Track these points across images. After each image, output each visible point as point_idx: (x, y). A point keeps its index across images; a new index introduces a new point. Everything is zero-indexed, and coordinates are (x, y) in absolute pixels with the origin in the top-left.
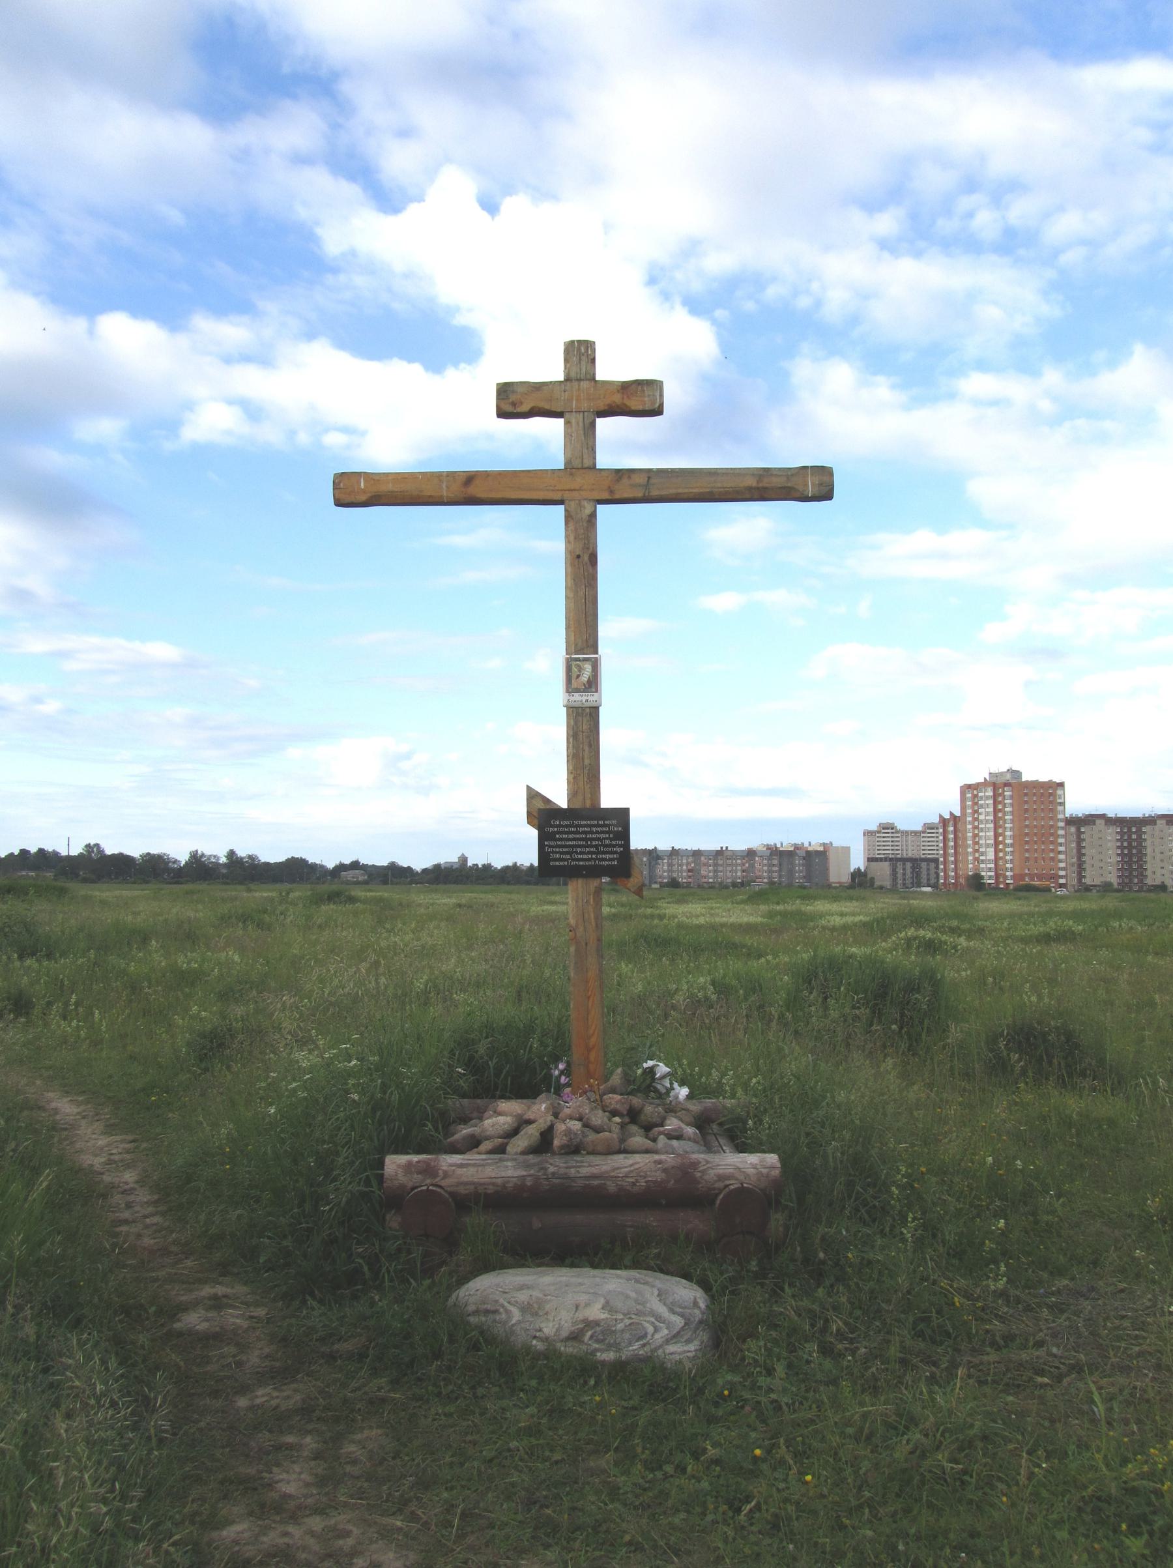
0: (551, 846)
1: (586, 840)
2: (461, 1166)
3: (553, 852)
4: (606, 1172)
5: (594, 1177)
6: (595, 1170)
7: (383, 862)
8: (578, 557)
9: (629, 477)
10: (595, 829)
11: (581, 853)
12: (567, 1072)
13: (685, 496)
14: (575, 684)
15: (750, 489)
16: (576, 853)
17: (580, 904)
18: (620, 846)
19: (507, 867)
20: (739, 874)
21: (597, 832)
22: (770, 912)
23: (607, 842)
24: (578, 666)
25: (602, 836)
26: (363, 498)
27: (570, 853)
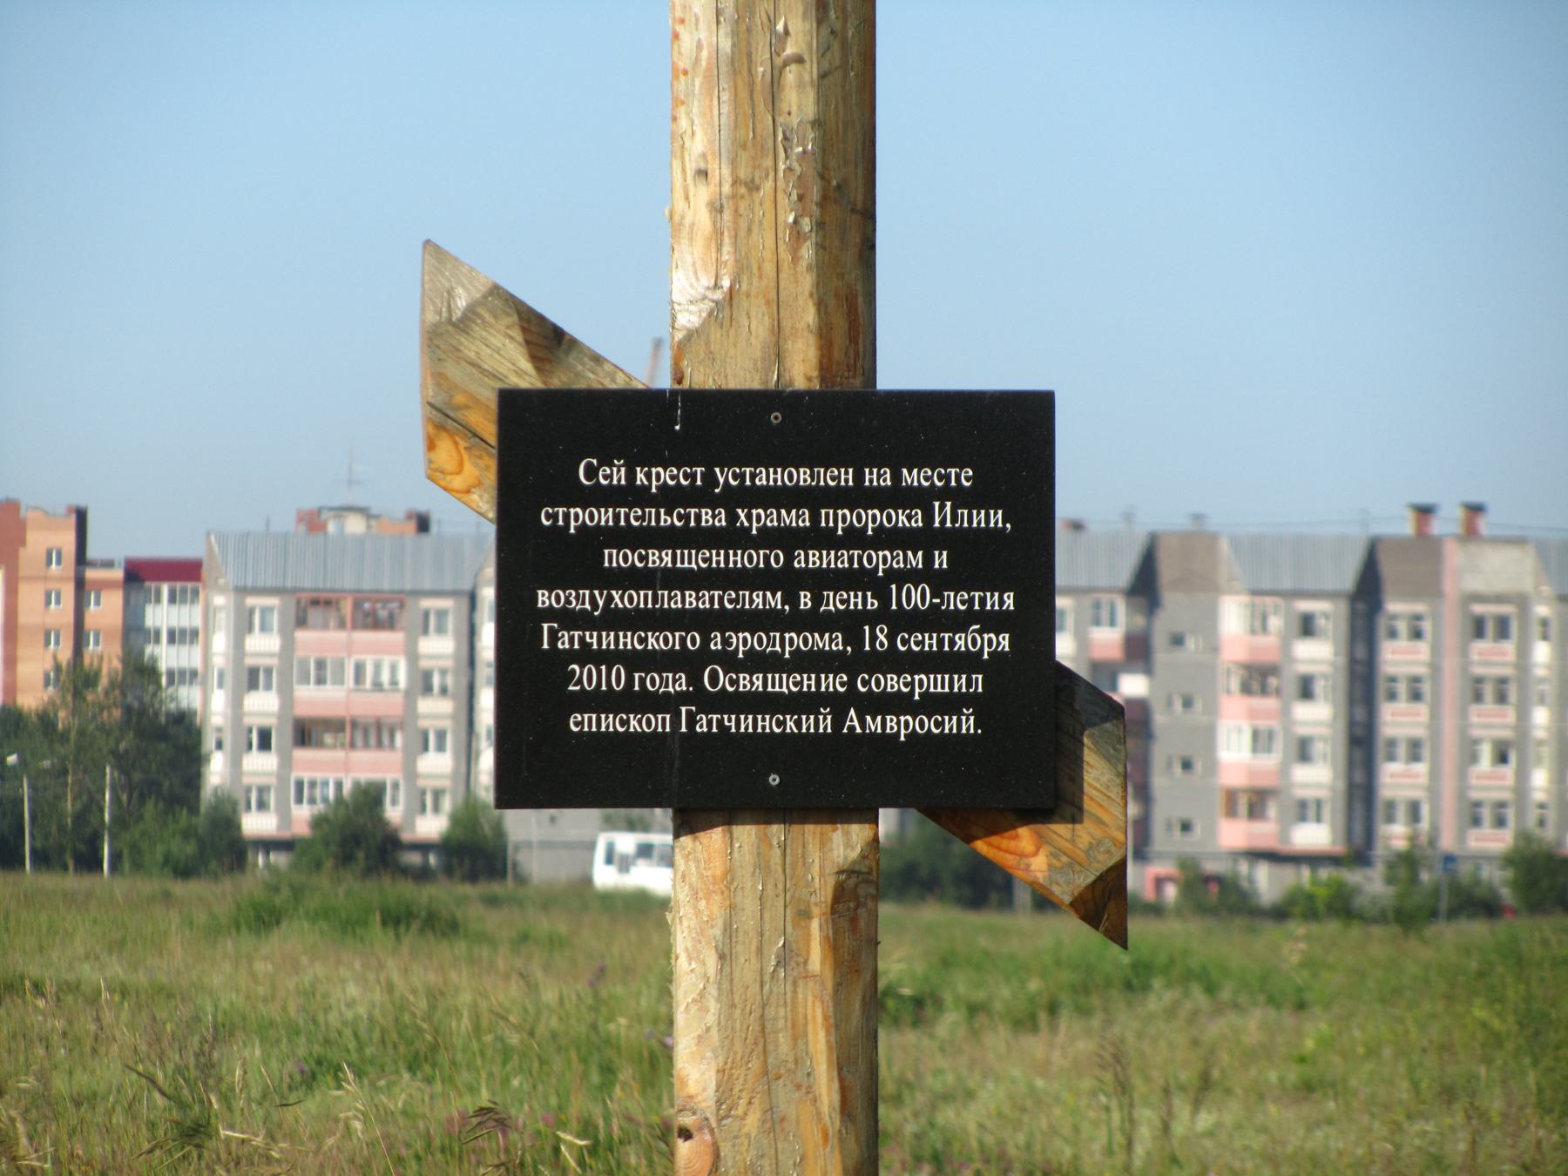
0: (569, 619)
1: (788, 581)
3: (586, 655)
10: (840, 519)
16: (729, 661)
17: (746, 970)
18: (993, 622)
21: (855, 538)
23: (917, 597)
25: (881, 560)
27: (689, 663)
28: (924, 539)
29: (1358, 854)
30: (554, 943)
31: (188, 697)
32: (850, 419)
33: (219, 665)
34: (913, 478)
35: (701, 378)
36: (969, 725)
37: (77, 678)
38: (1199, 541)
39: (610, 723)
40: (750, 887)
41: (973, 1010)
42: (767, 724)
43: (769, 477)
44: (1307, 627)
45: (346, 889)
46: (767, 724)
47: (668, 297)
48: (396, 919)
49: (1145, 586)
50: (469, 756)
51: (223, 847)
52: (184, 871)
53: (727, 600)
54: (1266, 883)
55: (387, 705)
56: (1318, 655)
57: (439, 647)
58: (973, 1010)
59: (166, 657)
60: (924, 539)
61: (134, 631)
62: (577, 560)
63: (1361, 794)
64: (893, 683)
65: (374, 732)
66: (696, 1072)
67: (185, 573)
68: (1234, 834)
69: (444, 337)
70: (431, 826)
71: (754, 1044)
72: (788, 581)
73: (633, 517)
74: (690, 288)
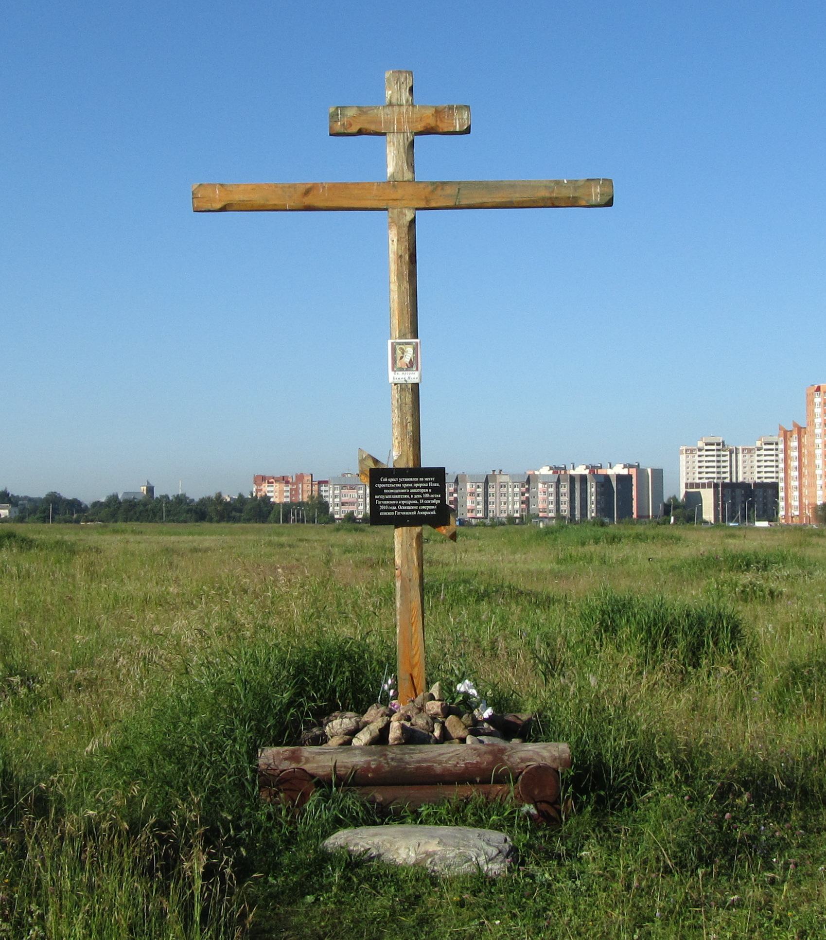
0: (380, 500)
1: (409, 494)
2: (319, 754)
3: (382, 504)
4: (434, 757)
5: (425, 761)
6: (423, 756)
7: (39, 492)
8: (401, 256)
9: (442, 189)
10: (416, 485)
11: (406, 505)
12: (394, 686)
13: (489, 205)
14: (399, 364)
15: (543, 199)
16: (401, 505)
17: (405, 547)
18: (437, 499)
19: (209, 499)
20: (517, 506)
21: (418, 488)
22: (47, 801)
23: (427, 496)
24: (401, 349)
25: (422, 491)
26: (219, 206)
27: (396, 505)
28: (428, 488)
29: (486, 517)
30: (377, 532)
31: (327, 499)
32: (418, 471)
33: (330, 494)
34: (426, 479)
35: (397, 466)
36: (434, 513)
37: (311, 497)
38: (464, 475)
39: (386, 514)
40: (405, 535)
41: (435, 541)
42: (407, 513)
43: (406, 480)
44: (478, 487)
45: (349, 526)
46: (407, 513)
47: (393, 454)
48: (356, 530)
49: (457, 481)
50: (365, 507)
51: (332, 520)
52: (327, 523)
53: (401, 496)
54: (474, 521)
55: (355, 500)
56: (480, 490)
57: (361, 492)
58: (435, 541)
59: (324, 494)
60: (428, 488)
61: (319, 490)
62: (381, 491)
63: (486, 508)
64: (424, 507)
65: (352, 504)
66: (398, 561)
67: (326, 482)
68: (469, 515)
69: (361, 461)
70: (360, 516)
71: (406, 558)
72: (409, 494)
73: (388, 485)
74: (395, 454)
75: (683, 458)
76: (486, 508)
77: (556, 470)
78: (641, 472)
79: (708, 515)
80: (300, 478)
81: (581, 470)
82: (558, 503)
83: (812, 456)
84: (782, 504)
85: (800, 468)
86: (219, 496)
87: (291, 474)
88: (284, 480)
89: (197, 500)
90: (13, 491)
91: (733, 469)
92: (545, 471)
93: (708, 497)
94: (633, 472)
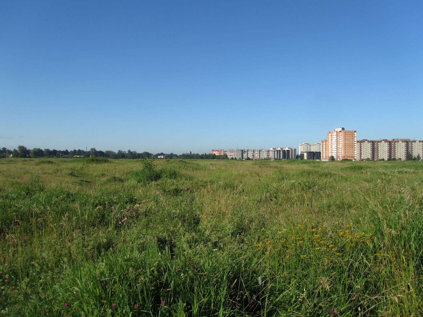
7: (169, 153)
19: (203, 155)
33: (228, 154)
51: (228, 159)
63: (260, 157)
75: (300, 146)
76: (260, 157)
77: (274, 149)
78: (292, 149)
79: (305, 158)
80: (221, 150)
81: (279, 149)
82: (274, 156)
83: (328, 146)
84: (322, 156)
85: (326, 149)
86: (206, 154)
87: (219, 149)
88: (218, 151)
89: (200, 155)
90: (164, 153)
91: (310, 149)
92: (272, 149)
93: (305, 154)
94: (290, 149)
